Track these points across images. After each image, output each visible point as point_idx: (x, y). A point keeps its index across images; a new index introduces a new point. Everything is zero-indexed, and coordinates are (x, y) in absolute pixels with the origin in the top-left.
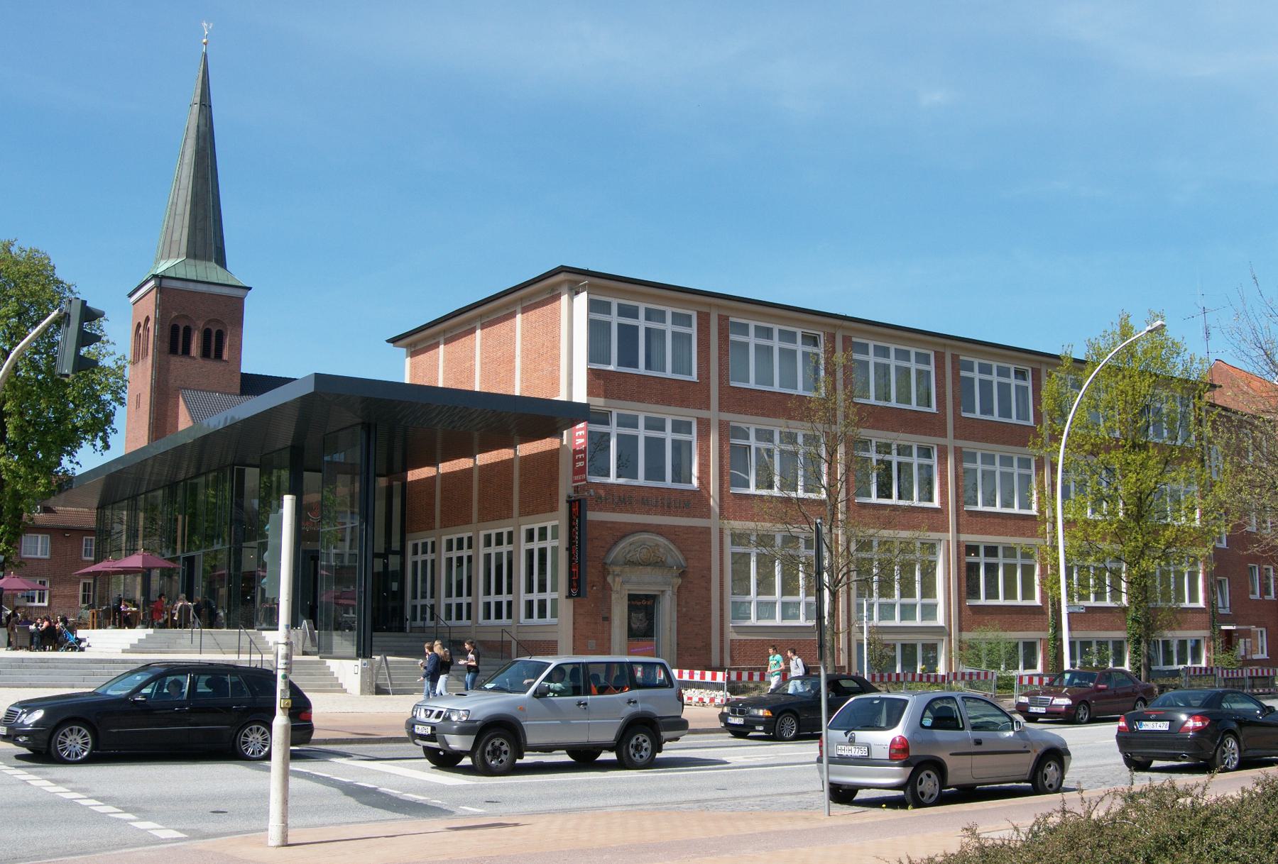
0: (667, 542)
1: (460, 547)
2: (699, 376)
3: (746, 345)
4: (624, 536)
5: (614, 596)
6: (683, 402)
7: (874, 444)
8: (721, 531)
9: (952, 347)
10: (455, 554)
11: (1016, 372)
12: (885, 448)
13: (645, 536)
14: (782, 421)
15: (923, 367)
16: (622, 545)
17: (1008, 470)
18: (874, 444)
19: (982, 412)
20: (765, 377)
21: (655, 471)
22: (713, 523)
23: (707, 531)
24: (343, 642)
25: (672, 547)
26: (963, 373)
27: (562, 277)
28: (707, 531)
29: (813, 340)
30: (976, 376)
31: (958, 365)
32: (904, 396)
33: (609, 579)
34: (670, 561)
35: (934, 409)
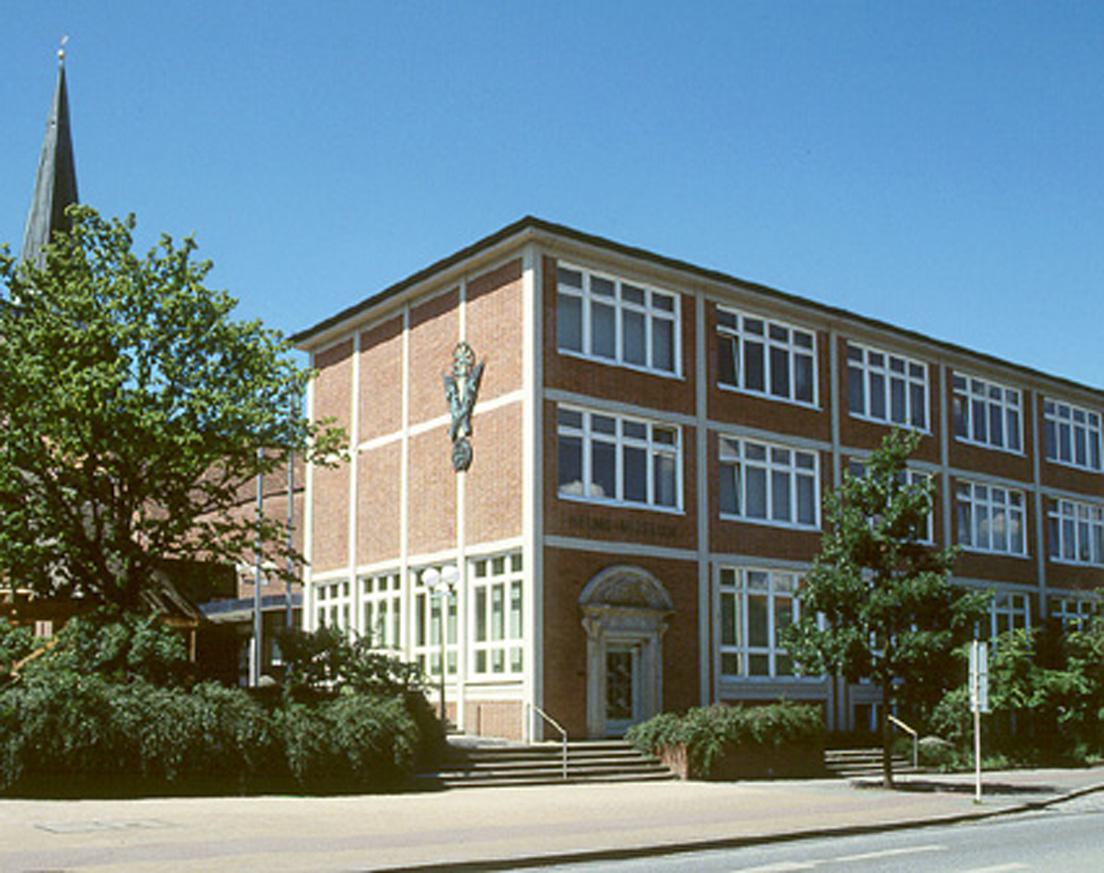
0: (651, 578)
1: (383, 586)
2: (685, 374)
3: (578, 301)
4: (601, 569)
5: (591, 645)
6: (666, 406)
7: (973, 487)
8: (710, 565)
9: (705, 288)
10: (376, 596)
11: (872, 355)
12: (603, 425)
13: (625, 569)
14: (656, 413)
15: (917, 381)
16: (599, 579)
17: (807, 472)
18: (973, 487)
19: (873, 414)
20: (604, 345)
21: (635, 490)
22: (702, 555)
23: (695, 565)
24: (427, 704)
25: (658, 584)
26: (852, 363)
27: (527, 232)
28: (695, 565)
29: (666, 303)
30: (866, 368)
31: (1043, 408)
32: (635, 353)
33: (585, 623)
34: (653, 600)
35: (815, 405)
